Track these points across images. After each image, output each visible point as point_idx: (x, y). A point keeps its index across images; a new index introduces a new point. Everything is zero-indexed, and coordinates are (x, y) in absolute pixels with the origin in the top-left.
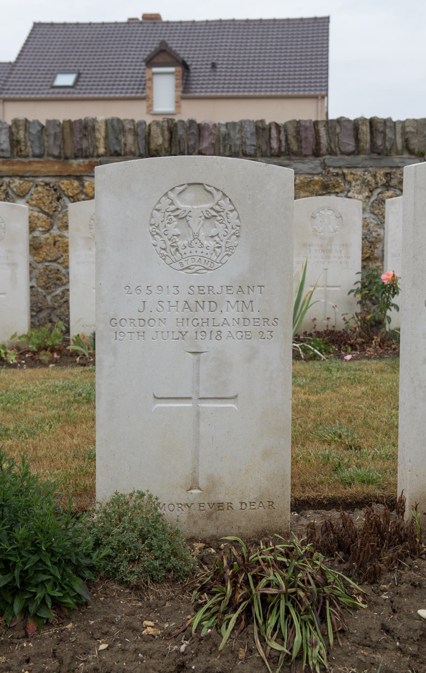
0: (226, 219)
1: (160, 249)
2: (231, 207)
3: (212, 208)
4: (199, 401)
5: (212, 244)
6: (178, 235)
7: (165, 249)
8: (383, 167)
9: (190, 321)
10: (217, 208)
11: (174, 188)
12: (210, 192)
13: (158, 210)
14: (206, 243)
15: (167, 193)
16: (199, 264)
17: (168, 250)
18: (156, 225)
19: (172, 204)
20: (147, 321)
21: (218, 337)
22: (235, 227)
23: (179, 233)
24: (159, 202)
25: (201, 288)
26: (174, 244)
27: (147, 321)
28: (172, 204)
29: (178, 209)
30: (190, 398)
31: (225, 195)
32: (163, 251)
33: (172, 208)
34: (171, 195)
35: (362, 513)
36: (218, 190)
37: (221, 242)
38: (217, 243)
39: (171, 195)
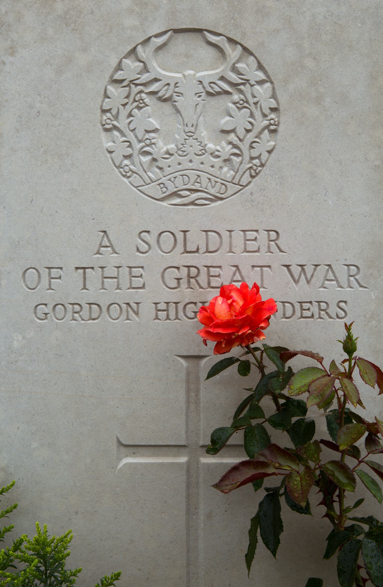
2: (261, 75)
3: (222, 78)
10: (233, 77)
14: (211, 146)
29: (156, 80)
32: (126, 162)
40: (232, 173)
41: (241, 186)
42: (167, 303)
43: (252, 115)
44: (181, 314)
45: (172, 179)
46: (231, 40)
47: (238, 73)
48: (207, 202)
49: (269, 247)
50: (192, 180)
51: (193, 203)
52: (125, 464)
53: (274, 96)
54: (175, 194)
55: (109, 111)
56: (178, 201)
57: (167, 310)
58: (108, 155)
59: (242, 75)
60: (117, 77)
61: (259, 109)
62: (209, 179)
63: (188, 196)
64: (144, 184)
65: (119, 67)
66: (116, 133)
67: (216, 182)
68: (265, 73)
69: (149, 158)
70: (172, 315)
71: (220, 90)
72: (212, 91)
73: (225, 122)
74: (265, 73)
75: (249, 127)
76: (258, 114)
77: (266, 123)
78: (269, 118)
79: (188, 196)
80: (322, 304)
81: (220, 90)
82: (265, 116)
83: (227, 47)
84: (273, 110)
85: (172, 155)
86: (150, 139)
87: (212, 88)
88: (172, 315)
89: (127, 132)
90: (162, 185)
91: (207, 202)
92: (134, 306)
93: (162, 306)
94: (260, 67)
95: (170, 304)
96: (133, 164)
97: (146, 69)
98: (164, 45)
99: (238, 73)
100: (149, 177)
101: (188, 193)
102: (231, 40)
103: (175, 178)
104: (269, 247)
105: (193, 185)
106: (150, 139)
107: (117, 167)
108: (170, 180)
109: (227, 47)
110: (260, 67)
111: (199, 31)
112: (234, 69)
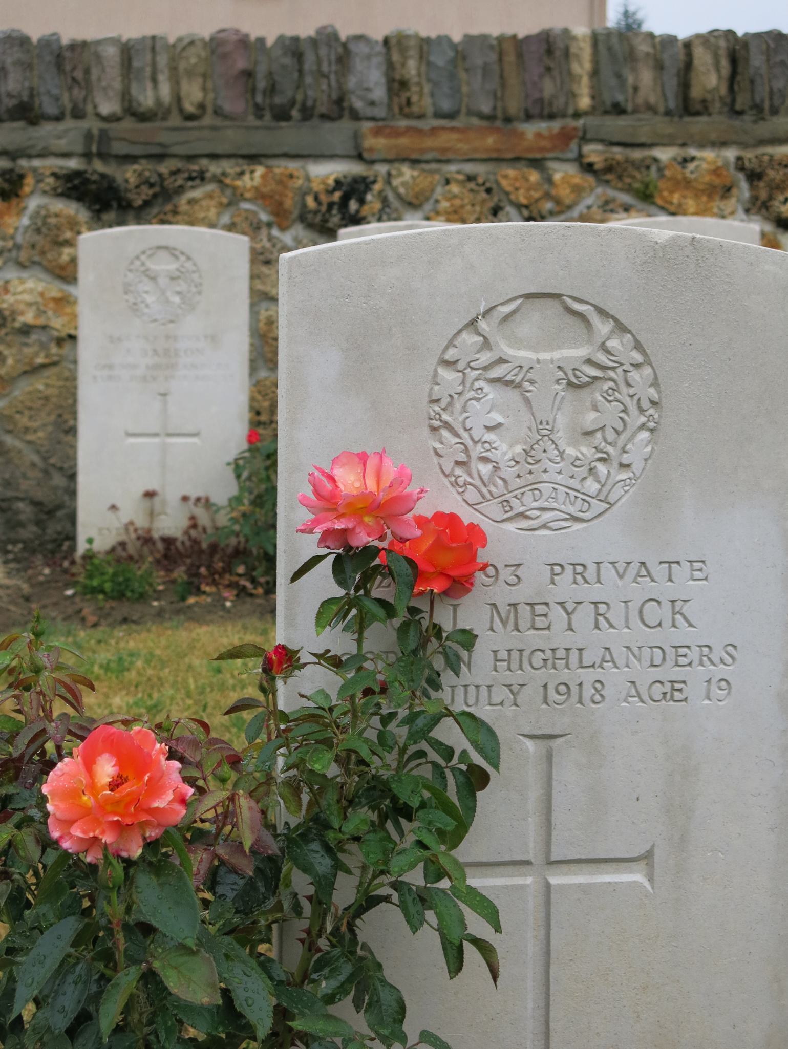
2: (638, 357)
3: (589, 362)
10: (602, 358)
13: (450, 364)
14: (571, 451)
28: (486, 344)
29: (501, 361)
30: (528, 863)
32: (458, 471)
33: (485, 358)
34: (483, 325)
40: (598, 486)
41: (608, 503)
42: (509, 651)
43: (625, 411)
44: (526, 665)
45: (519, 496)
46: (601, 312)
47: (608, 352)
48: (564, 524)
49: (673, 620)
50: (544, 497)
51: (544, 526)
52: (315, 962)
53: (655, 384)
54: (522, 515)
55: (438, 401)
56: (525, 524)
57: (567, 658)
58: (435, 460)
59: (614, 355)
60: (448, 356)
61: (635, 402)
62: (567, 493)
63: (538, 517)
64: (481, 500)
65: (451, 344)
66: (445, 433)
67: (576, 497)
68: (643, 352)
69: (490, 467)
70: (515, 666)
71: (587, 379)
72: (576, 381)
73: (590, 419)
74: (643, 352)
75: (620, 427)
76: (632, 406)
77: (643, 419)
78: (647, 413)
79: (538, 517)
80: (600, 606)
81: (587, 379)
82: (642, 411)
83: (595, 319)
84: (654, 403)
85: (517, 462)
86: (489, 443)
87: (577, 377)
88: (515, 666)
89: (461, 432)
90: (505, 504)
91: (564, 524)
92: (636, 650)
93: (503, 655)
94: (638, 346)
95: (571, 652)
96: (470, 475)
97: (486, 344)
98: (514, 312)
99: (608, 352)
100: (490, 492)
101: (537, 513)
102: (601, 312)
103: (523, 494)
104: (673, 620)
105: (546, 501)
106: (489, 443)
107: (446, 476)
108: (516, 497)
109: (595, 319)
110: (638, 346)
111: (558, 296)
112: (604, 348)
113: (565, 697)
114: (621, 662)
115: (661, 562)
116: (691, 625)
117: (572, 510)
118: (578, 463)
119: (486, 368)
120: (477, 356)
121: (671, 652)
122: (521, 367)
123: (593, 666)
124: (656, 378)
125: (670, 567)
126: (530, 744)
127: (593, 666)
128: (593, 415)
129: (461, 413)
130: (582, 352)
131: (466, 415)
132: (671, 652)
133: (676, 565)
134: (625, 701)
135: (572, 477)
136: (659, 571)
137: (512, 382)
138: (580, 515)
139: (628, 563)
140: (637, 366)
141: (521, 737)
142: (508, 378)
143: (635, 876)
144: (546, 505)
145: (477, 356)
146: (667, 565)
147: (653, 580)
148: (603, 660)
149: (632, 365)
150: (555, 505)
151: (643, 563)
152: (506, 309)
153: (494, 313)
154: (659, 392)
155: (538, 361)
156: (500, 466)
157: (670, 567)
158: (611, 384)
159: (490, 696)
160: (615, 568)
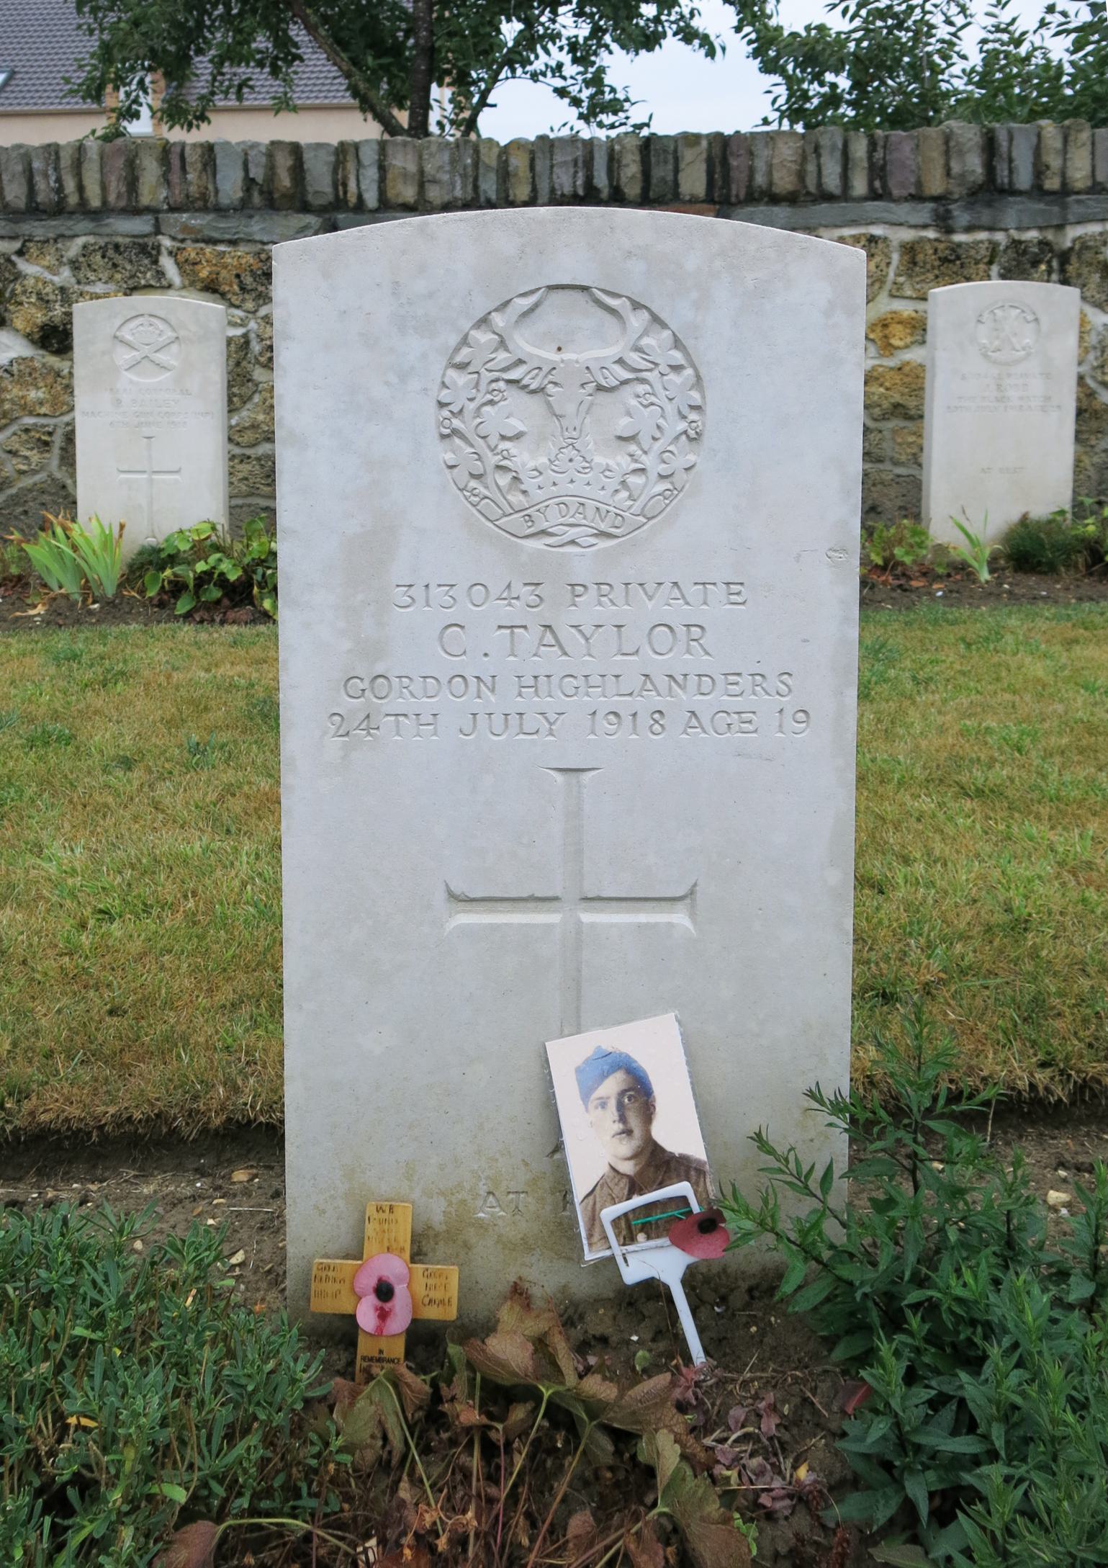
0: (662, 393)
1: (467, 476)
2: (678, 357)
3: (620, 361)
4: (584, 905)
5: (621, 461)
6: (518, 436)
7: (478, 477)
8: (532, 168)
9: (555, 680)
10: (634, 359)
11: (509, 302)
12: (612, 311)
13: (462, 367)
14: (599, 460)
15: (664, 325)
16: (579, 519)
17: (489, 480)
18: (455, 408)
19: (502, 344)
20: (444, 680)
21: (657, 728)
22: (685, 411)
23: (522, 428)
24: (465, 341)
25: (735, 588)
26: (504, 463)
27: (444, 680)
28: (502, 344)
29: (521, 362)
30: (556, 899)
31: (656, 319)
32: (473, 483)
33: (502, 357)
34: (498, 320)
35: (450, 1345)
36: (637, 306)
37: (644, 458)
38: (636, 461)
39: (498, 320)
50: (571, 513)
51: (573, 542)
56: (551, 540)
69: (510, 475)
92: (680, 678)
94: (677, 344)
107: (461, 490)
110: (677, 344)
111: (584, 289)
113: (804, 725)
114: (664, 691)
115: (500, 627)
116: (707, 653)
117: (603, 527)
118: (607, 473)
119: (505, 370)
120: (493, 356)
121: (720, 679)
122: (540, 368)
123: (631, 694)
124: (698, 377)
125: (512, 633)
126: (559, 777)
127: (631, 694)
128: (627, 420)
129: (475, 418)
130: (613, 351)
131: (479, 420)
132: (720, 679)
133: (521, 630)
134: (685, 732)
135: (603, 488)
136: (693, 592)
137: (526, 386)
138: (613, 531)
139: (660, 584)
140: (677, 368)
141: (552, 772)
142: (524, 382)
143: (679, 918)
144: (572, 521)
145: (493, 356)
146: (508, 631)
147: (687, 603)
148: (643, 689)
149: (670, 366)
150: (584, 522)
151: (675, 584)
152: (527, 302)
153: (509, 309)
154: (703, 397)
155: (563, 361)
156: (520, 476)
157: (512, 633)
158: (647, 387)
159: (521, 724)
160: (644, 590)
